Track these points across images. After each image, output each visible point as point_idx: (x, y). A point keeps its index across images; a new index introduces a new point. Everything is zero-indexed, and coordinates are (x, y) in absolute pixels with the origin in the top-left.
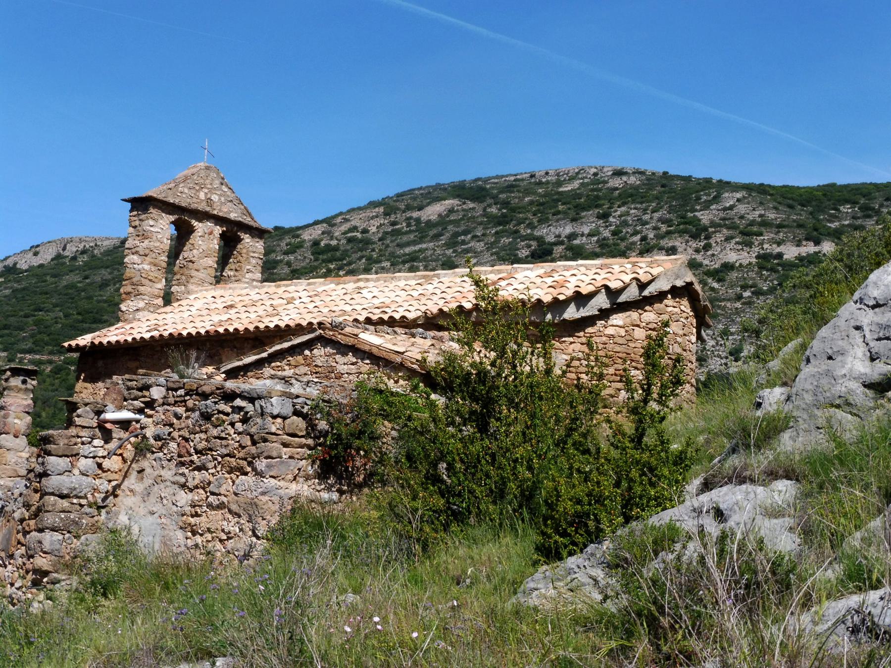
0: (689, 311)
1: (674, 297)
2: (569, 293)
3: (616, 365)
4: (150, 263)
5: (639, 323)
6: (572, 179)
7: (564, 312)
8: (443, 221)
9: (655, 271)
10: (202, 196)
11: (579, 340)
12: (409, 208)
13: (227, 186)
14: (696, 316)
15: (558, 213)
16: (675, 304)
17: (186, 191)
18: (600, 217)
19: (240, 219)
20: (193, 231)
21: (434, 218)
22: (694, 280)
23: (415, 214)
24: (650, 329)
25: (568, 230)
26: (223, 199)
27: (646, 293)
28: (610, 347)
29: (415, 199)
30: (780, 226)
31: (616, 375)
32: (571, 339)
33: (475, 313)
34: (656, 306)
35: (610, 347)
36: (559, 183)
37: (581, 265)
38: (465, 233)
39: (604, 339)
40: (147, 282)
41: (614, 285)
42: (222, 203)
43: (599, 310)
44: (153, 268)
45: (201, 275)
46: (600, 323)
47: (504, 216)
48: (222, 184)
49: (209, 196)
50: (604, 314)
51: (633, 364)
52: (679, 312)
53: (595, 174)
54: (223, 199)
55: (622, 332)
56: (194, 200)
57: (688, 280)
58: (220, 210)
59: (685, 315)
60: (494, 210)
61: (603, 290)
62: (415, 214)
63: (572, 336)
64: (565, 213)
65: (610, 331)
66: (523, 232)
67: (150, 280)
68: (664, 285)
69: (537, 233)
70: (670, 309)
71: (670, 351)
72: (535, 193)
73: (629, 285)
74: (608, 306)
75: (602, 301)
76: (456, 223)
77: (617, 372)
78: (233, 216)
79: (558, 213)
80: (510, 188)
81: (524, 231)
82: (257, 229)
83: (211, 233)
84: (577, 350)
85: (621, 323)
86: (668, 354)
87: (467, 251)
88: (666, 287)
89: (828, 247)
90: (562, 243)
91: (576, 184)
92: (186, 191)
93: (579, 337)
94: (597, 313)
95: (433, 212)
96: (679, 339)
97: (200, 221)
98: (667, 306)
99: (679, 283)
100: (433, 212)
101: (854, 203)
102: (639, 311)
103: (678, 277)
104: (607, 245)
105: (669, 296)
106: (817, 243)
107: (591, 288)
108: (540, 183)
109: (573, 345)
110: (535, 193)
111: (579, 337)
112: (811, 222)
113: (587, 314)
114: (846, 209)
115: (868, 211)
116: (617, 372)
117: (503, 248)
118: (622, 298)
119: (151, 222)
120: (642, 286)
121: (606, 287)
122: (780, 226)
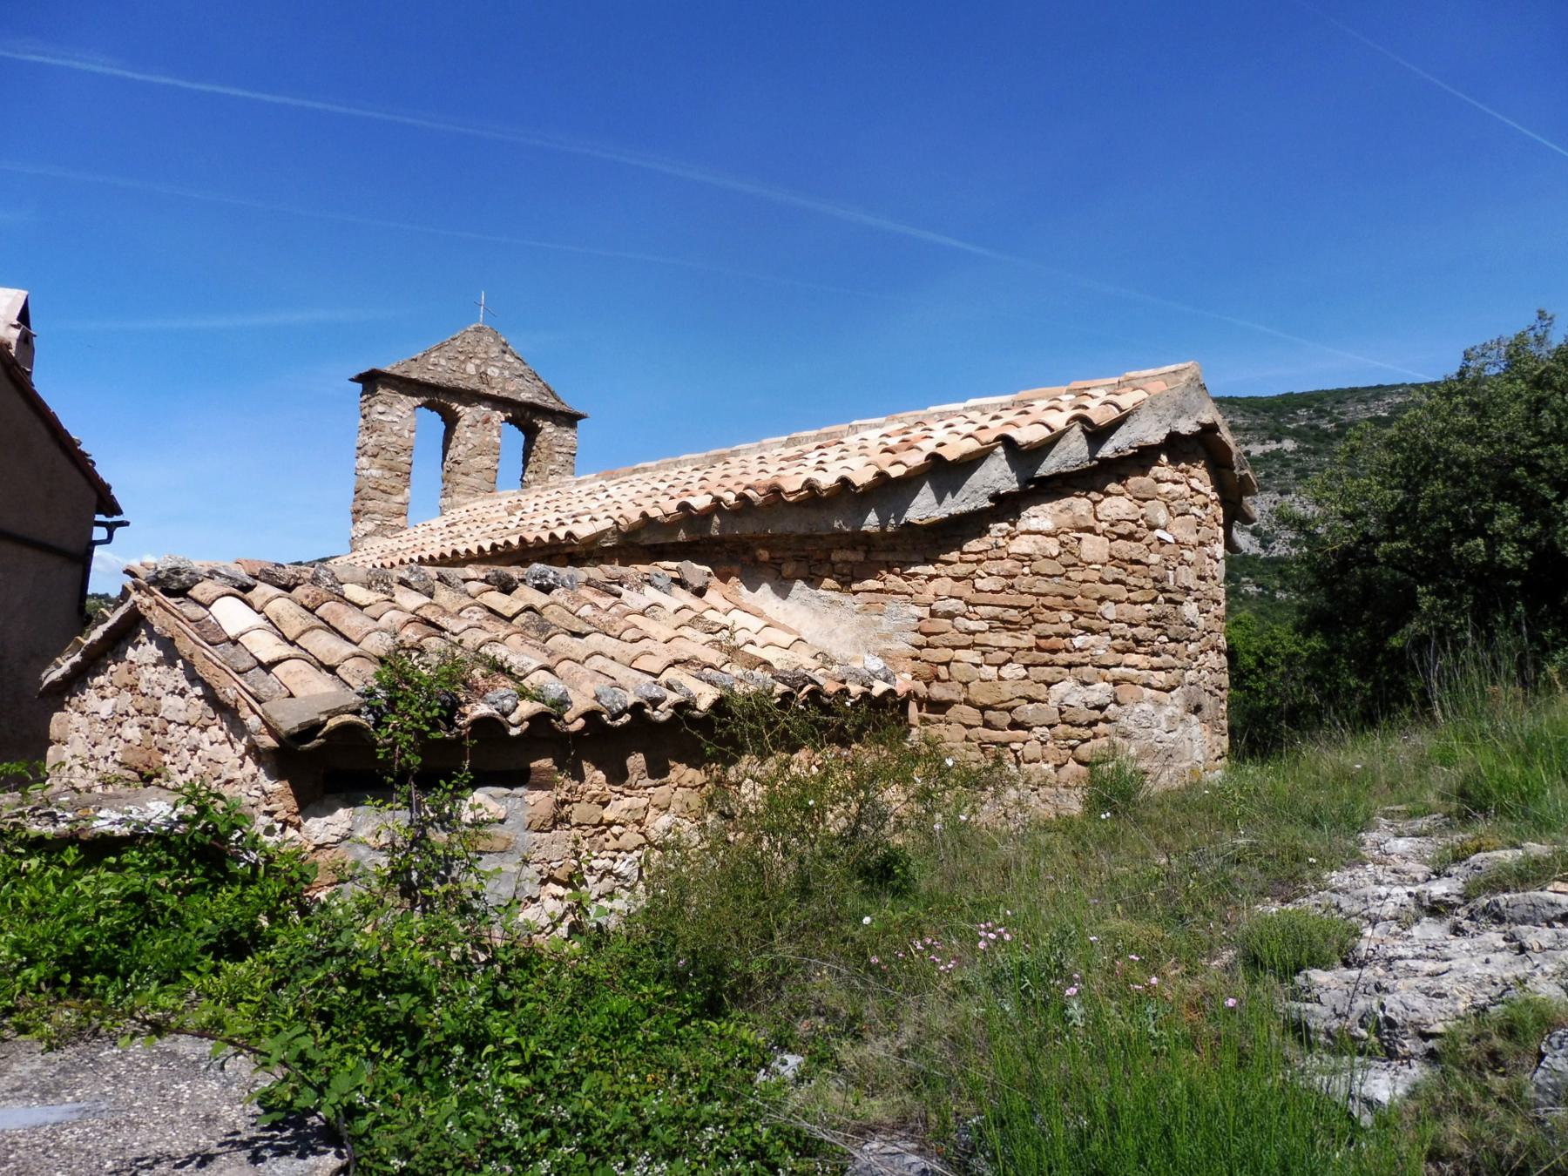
0: (1208, 489)
1: (1174, 460)
2: (916, 459)
3: (1039, 627)
4: (382, 467)
5: (1092, 522)
7: (907, 505)
9: (1127, 400)
10: (471, 368)
11: (949, 570)
13: (512, 354)
14: (1223, 502)
16: (1177, 476)
17: (443, 362)
19: (537, 401)
20: (458, 420)
22: (1219, 419)
24: (1120, 536)
26: (506, 373)
27: (1107, 451)
28: (1023, 582)
30: (1247, 430)
31: (1039, 648)
32: (931, 570)
33: (716, 519)
34: (1134, 481)
35: (1023, 582)
37: (973, 408)
39: (1009, 565)
40: (378, 494)
41: (1027, 434)
42: (505, 379)
43: (991, 498)
44: (387, 474)
45: (472, 480)
46: (998, 528)
50: (1006, 507)
51: (1082, 620)
52: (1188, 493)
54: (506, 373)
55: (1052, 547)
56: (458, 375)
57: (1207, 418)
58: (503, 389)
59: (1200, 499)
61: (1000, 450)
63: (933, 562)
65: (1023, 545)
67: (384, 491)
68: (1148, 431)
70: (1165, 488)
71: (1170, 585)
73: (1063, 433)
74: (1014, 486)
75: (997, 475)
77: (1042, 643)
78: (525, 397)
82: (561, 413)
83: (487, 421)
84: (944, 593)
85: (1047, 525)
86: (1164, 590)
88: (1156, 436)
89: (1289, 445)
92: (443, 362)
93: (948, 563)
94: (988, 504)
96: (1188, 555)
97: (467, 405)
98: (1158, 480)
99: (1186, 427)
101: (1308, 407)
102: (1094, 495)
103: (1181, 412)
105: (1164, 458)
106: (1279, 441)
107: (971, 445)
109: (934, 583)
111: (948, 563)
112: (1273, 425)
113: (964, 508)
114: (1302, 412)
115: (1321, 413)
116: (1042, 643)
118: (1048, 467)
119: (380, 408)
120: (1097, 435)
121: (1006, 441)
122: (1247, 430)
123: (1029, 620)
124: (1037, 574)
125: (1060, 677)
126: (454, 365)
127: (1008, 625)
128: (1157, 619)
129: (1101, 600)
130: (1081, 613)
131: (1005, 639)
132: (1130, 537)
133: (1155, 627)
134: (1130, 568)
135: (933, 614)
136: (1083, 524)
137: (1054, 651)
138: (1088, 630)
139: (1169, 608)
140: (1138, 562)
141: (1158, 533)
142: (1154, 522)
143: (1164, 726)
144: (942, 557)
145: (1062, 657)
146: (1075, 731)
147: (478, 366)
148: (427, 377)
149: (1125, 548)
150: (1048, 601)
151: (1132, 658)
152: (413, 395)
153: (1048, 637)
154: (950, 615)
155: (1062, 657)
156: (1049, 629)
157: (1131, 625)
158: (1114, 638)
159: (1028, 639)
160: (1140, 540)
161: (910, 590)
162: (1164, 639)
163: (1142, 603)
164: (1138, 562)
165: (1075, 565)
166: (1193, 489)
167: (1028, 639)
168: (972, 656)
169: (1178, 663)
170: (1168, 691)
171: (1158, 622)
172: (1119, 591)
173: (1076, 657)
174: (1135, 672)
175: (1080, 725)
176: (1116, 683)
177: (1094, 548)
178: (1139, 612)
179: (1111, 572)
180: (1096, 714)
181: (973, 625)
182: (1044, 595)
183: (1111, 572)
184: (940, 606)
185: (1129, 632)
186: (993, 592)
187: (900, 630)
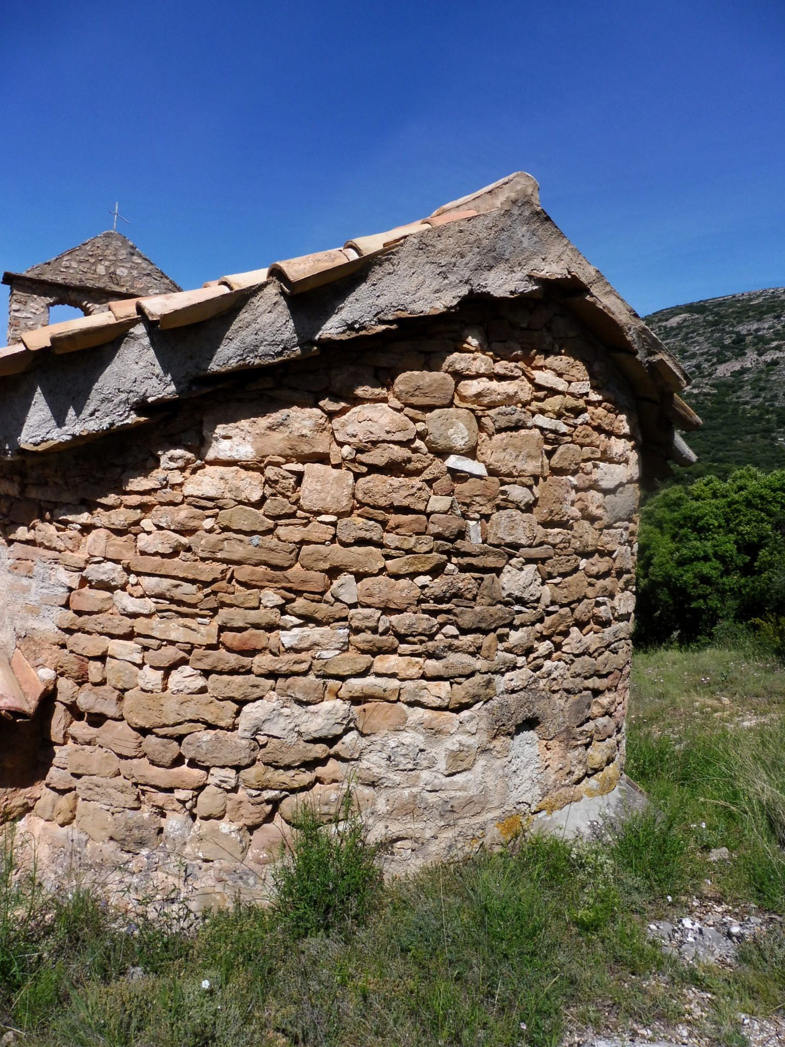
6: (758, 296)
8: (680, 327)
10: (101, 269)
12: (660, 320)
13: (140, 256)
15: (749, 317)
17: (74, 265)
18: (775, 317)
21: (674, 325)
23: (664, 324)
24: (373, 469)
25: (755, 326)
29: (663, 315)
36: (750, 300)
38: (693, 332)
39: (183, 513)
42: (134, 278)
47: (716, 321)
48: (133, 254)
49: (112, 269)
53: (773, 293)
54: (135, 273)
56: (89, 275)
58: (132, 287)
60: (710, 318)
62: (664, 324)
64: (753, 316)
65: (206, 482)
66: (727, 330)
69: (736, 330)
72: (735, 307)
75: (136, 375)
76: (688, 327)
79: (749, 317)
80: (720, 304)
81: (728, 328)
85: (245, 451)
87: (694, 342)
90: (751, 334)
91: (761, 299)
92: (74, 265)
94: (133, 418)
95: (674, 321)
96: (517, 493)
98: (459, 376)
100: (674, 321)
103: (493, 258)
104: (779, 334)
108: (739, 301)
110: (735, 307)
113: (93, 426)
117: (715, 340)
118: (226, 356)
123: (212, 602)
124: (226, 529)
125: (258, 692)
126: (84, 267)
127: (182, 608)
128: (438, 600)
129: (334, 572)
130: (299, 593)
131: (175, 629)
132: (393, 468)
133: (434, 613)
134: (394, 519)
135: (84, 582)
136: (307, 449)
137: (252, 653)
138: (307, 619)
139: (466, 581)
140: (406, 510)
141: (453, 461)
142: (442, 443)
143: (442, 765)
144: (103, 501)
145: (263, 662)
146: (284, 777)
147: (107, 267)
148: (59, 279)
149: (382, 487)
150: (243, 573)
151: (390, 662)
152: (45, 296)
153: (240, 630)
154: (107, 586)
155: (263, 662)
156: (237, 617)
157: (387, 611)
158: (357, 631)
159: (206, 631)
160: (418, 472)
161: (60, 545)
162: (451, 630)
163: (413, 575)
164: (406, 510)
165: (293, 515)
166: (539, 387)
167: (206, 631)
168: (128, 650)
169: (479, 664)
170: (457, 710)
171: (441, 604)
172: (372, 558)
173: (283, 663)
174: (395, 683)
175: (288, 767)
176: (356, 701)
177: (324, 486)
178: (405, 590)
179: (357, 525)
180: (319, 750)
181: (133, 605)
182: (239, 563)
183: (357, 525)
184: (95, 573)
185: (385, 622)
186: (163, 556)
187: (47, 603)
